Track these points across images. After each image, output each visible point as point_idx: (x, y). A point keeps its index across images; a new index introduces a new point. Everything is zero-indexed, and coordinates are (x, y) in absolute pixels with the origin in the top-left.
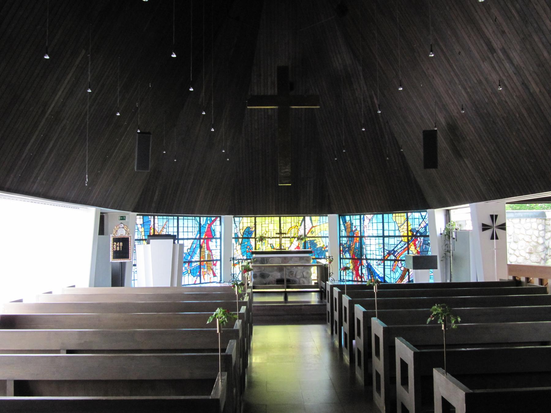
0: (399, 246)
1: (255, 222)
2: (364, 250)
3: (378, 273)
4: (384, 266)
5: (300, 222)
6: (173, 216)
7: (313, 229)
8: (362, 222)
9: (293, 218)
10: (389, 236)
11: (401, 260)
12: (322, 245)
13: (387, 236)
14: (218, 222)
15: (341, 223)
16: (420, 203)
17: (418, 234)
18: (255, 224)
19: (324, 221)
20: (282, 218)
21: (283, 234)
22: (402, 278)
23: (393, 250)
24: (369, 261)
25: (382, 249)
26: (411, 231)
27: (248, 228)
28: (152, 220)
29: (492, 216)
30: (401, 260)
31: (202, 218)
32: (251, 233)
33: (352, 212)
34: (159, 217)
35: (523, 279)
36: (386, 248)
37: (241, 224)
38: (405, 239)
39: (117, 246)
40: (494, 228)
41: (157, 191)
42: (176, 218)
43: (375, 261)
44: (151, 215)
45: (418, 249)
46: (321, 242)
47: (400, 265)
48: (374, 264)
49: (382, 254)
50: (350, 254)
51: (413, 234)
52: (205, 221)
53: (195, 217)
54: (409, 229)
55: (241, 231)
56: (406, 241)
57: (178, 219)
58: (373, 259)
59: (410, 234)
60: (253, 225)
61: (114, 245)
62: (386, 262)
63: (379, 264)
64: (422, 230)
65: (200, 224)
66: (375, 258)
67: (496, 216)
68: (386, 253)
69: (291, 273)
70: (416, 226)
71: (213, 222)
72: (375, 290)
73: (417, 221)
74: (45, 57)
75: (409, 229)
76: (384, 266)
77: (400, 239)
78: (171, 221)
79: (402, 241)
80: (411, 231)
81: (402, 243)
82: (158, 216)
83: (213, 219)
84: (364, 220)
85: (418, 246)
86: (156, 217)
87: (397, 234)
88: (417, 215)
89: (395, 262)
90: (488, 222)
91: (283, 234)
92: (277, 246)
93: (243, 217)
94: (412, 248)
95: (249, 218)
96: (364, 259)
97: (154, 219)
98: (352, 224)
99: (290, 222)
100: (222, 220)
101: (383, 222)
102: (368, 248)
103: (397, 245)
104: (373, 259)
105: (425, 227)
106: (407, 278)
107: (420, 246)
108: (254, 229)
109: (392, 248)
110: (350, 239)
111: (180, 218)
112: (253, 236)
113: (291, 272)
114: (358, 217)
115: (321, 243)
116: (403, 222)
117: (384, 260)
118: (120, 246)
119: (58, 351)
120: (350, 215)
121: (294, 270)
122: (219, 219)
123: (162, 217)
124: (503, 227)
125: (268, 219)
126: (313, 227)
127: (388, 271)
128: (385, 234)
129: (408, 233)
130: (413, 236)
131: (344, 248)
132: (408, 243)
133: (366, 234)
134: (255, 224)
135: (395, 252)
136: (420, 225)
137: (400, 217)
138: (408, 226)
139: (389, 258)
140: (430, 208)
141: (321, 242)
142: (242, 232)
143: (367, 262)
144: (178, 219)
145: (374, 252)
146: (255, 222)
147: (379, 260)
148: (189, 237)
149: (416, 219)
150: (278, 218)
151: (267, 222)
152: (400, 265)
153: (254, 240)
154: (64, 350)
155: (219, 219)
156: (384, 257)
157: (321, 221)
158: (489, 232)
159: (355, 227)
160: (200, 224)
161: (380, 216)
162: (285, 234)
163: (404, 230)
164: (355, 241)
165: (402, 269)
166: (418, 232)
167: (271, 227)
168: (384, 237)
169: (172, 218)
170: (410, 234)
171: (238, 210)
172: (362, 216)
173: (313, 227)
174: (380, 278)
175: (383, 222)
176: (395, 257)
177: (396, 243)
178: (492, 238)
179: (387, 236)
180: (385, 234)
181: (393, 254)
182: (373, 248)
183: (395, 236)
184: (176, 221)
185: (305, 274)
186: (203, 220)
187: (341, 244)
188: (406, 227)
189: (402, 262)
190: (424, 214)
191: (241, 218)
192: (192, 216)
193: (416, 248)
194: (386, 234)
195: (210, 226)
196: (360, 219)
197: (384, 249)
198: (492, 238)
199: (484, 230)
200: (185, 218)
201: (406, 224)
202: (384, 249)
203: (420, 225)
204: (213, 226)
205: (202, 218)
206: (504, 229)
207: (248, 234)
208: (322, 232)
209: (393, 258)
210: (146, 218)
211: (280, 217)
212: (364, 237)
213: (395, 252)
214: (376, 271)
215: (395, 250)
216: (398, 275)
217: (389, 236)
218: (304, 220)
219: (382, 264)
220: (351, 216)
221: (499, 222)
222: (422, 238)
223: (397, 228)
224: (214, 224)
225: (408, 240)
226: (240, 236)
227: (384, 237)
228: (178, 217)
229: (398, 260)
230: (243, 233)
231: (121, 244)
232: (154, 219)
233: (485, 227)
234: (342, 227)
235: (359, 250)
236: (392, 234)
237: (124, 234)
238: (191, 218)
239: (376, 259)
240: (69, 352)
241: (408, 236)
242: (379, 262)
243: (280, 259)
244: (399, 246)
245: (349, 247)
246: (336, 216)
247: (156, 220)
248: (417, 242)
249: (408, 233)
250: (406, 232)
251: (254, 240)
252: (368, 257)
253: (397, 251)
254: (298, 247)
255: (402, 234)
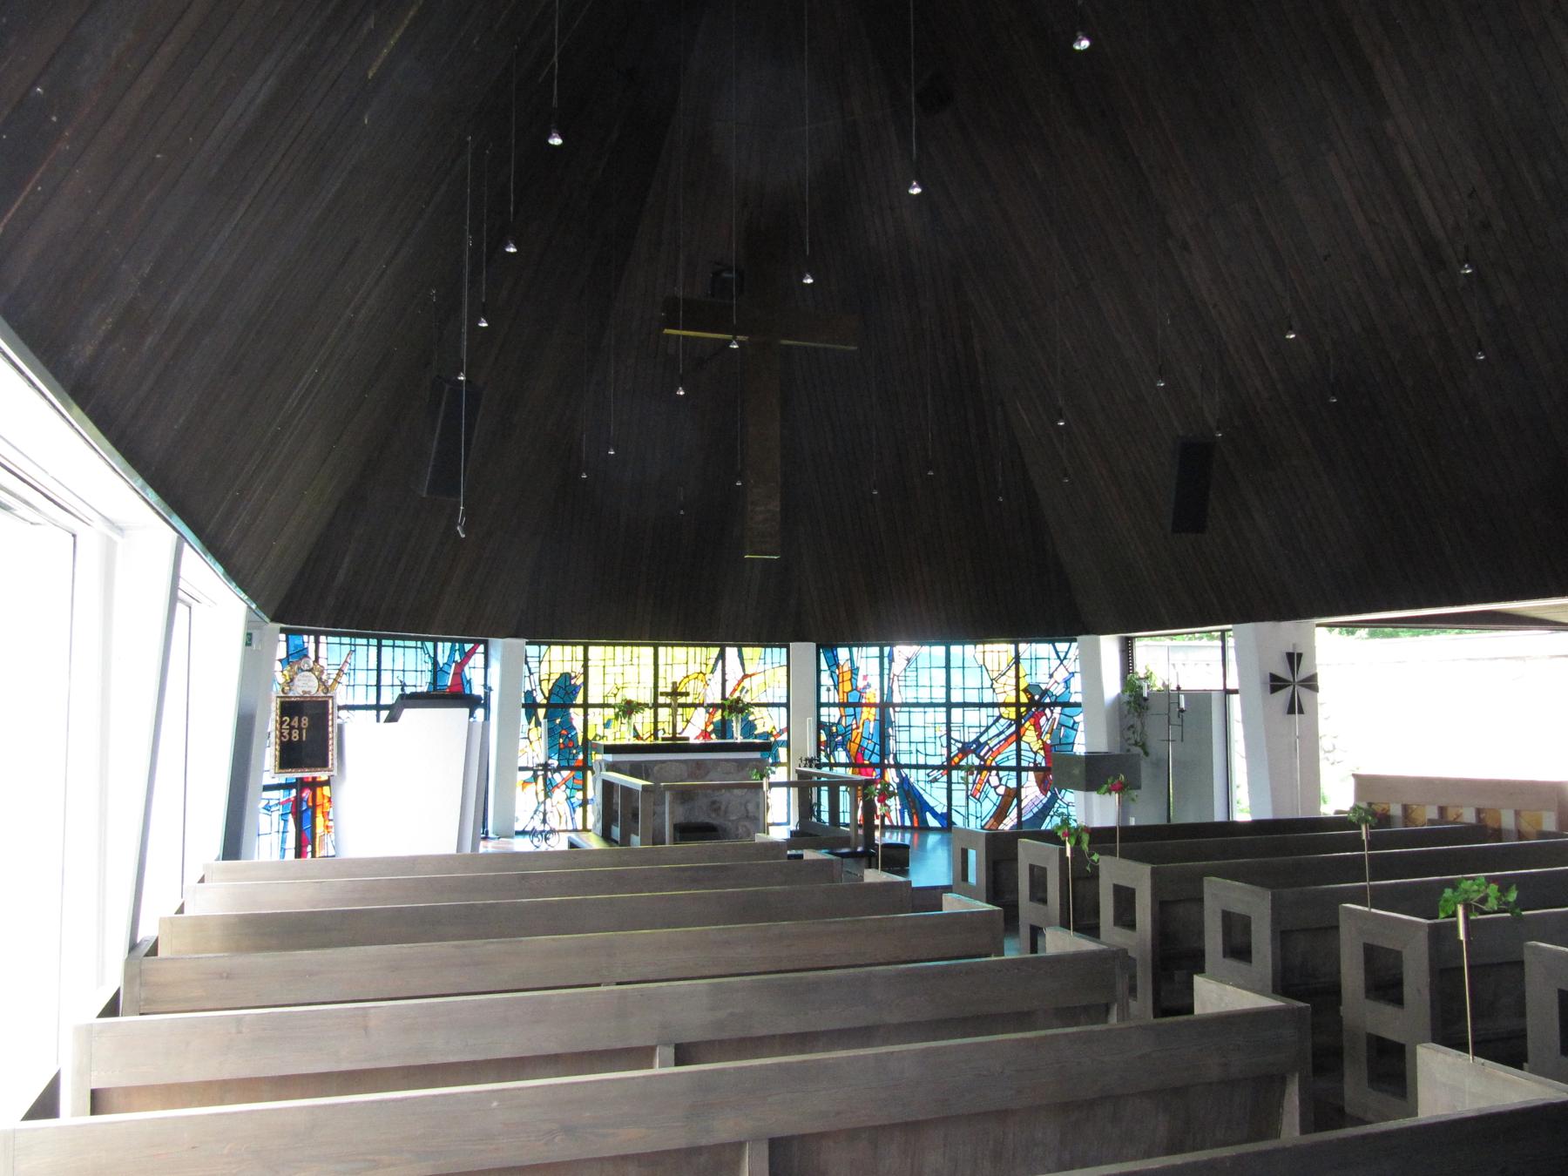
0: (993, 731)
1: (586, 659)
2: (892, 742)
3: (932, 803)
4: (949, 782)
5: (712, 662)
6: (368, 637)
7: (746, 683)
8: (886, 665)
9: (691, 649)
10: (964, 705)
11: (999, 768)
12: (769, 729)
13: (958, 705)
14: (478, 659)
15: (824, 666)
16: (1060, 619)
17: (1047, 700)
18: (585, 666)
19: (776, 659)
20: (661, 650)
21: (682, 694)
22: (1001, 813)
23: (977, 740)
24: (906, 771)
25: (944, 739)
26: (1025, 691)
27: (566, 677)
28: (311, 647)
29: (1290, 656)
30: (999, 768)
31: (440, 644)
32: (575, 689)
33: (856, 638)
34: (331, 639)
35: (1396, 810)
36: (955, 735)
37: (545, 665)
38: (1011, 713)
39: (292, 728)
40: (1290, 685)
41: (347, 559)
42: (374, 642)
43: (922, 772)
44: (309, 633)
45: (1047, 738)
46: (767, 719)
47: (994, 781)
48: (917, 778)
49: (945, 751)
50: (848, 752)
51: (1031, 699)
52: (447, 652)
53: (423, 640)
54: (1022, 686)
55: (544, 684)
56: (1013, 716)
57: (379, 647)
58: (918, 767)
59: (1024, 699)
60: (579, 668)
61: (282, 723)
62: (954, 773)
63: (936, 780)
64: (1058, 690)
65: (435, 663)
66: (922, 762)
67: (1300, 656)
68: (954, 749)
69: (715, 807)
70: (1042, 679)
71: (467, 656)
72: (1364, 831)
73: (1043, 665)
74: (551, 142)
75: (1022, 686)
76: (949, 782)
77: (996, 712)
78: (361, 651)
79: (1000, 716)
80: (1025, 691)
81: (1002, 721)
82: (327, 634)
83: (468, 647)
84: (891, 660)
85: (1046, 728)
86: (322, 638)
87: (988, 697)
88: (1043, 649)
89: (980, 773)
90: (1282, 671)
91: (682, 694)
92: (665, 730)
93: (549, 644)
94: (1030, 736)
95: (568, 649)
96: (890, 766)
97: (317, 642)
98: (854, 671)
99: (684, 663)
100: (492, 651)
101: (948, 667)
102: (903, 736)
103: (988, 728)
104: (918, 767)
105: (1067, 682)
106: (1013, 814)
107: (1051, 732)
108: (580, 681)
109: (973, 737)
110: (850, 711)
111: (384, 642)
112: (579, 700)
113: (714, 803)
114: (875, 651)
115: (768, 722)
116: (1004, 667)
117: (948, 767)
118: (300, 729)
119: (640, 1056)
120: (850, 647)
121: (725, 796)
122: (481, 648)
123: (336, 640)
124: (1311, 683)
125: (622, 653)
126: (745, 676)
127: (959, 797)
128: (954, 700)
129: (1018, 696)
130: (1032, 703)
131: (830, 735)
132: (1018, 722)
133: (897, 699)
134: (585, 666)
135: (980, 746)
136: (1051, 676)
137: (999, 653)
138: (1017, 677)
139: (963, 763)
140: (1088, 633)
141: (767, 719)
142: (546, 687)
143: (899, 775)
144: (379, 647)
145: (921, 747)
146: (586, 659)
147: (934, 767)
148: (968, 700)
149: (1046, 663)
150: (651, 650)
151: (619, 661)
152: (994, 781)
153: (580, 711)
154: (666, 1044)
155: (481, 648)
156: (949, 758)
157: (768, 660)
158: (1283, 696)
159: (865, 677)
160: (435, 663)
161: (939, 651)
162: (687, 694)
163: (1007, 688)
164: (864, 716)
165: (1001, 790)
166: (1045, 693)
167: (631, 672)
168: (949, 705)
169: (364, 641)
170: (1024, 699)
171: (545, 627)
172: (887, 650)
173: (745, 676)
174: (935, 815)
175: (948, 667)
176: (982, 758)
177: (984, 723)
178: (1291, 711)
179: (958, 705)
180: (954, 700)
181: (976, 752)
182: (917, 735)
183: (981, 705)
184: (373, 650)
185: (750, 807)
186: (444, 650)
187: (820, 725)
188: (1013, 681)
189: (1002, 773)
190: (1062, 647)
191: (544, 648)
192: (416, 639)
193: (1039, 736)
194: (956, 697)
195: (460, 666)
196: (881, 657)
197: (949, 738)
198: (1291, 711)
199: (1274, 689)
200: (398, 643)
201: (1012, 672)
202: (949, 738)
203: (1051, 676)
204: (466, 668)
205: (440, 644)
206: (1315, 688)
207: (564, 695)
208: (770, 691)
209: (977, 762)
210: (296, 640)
211: (656, 648)
212: (894, 706)
213: (980, 746)
214: (926, 797)
215: (982, 740)
216: (988, 807)
217: (964, 705)
218: (722, 656)
219: (945, 778)
220: (855, 650)
221: (1303, 673)
222: (1058, 710)
223: (987, 683)
224: (471, 663)
225: (1018, 713)
226: (540, 699)
227: (949, 705)
228: (379, 640)
229: (990, 769)
230: (551, 692)
231: (305, 721)
232: (317, 642)
233: (1276, 684)
234: (826, 679)
235: (876, 739)
236: (972, 697)
237: (313, 691)
238: (412, 643)
239: (925, 767)
240: (683, 1055)
241: (1018, 704)
242: (936, 773)
243: (684, 767)
244: (993, 731)
245: (847, 731)
246: (813, 645)
247: (322, 647)
248: (1043, 721)
249: (1018, 696)
250: (1014, 693)
251: (580, 711)
252: (904, 759)
253: (986, 743)
254: (705, 734)
255: (1001, 699)
